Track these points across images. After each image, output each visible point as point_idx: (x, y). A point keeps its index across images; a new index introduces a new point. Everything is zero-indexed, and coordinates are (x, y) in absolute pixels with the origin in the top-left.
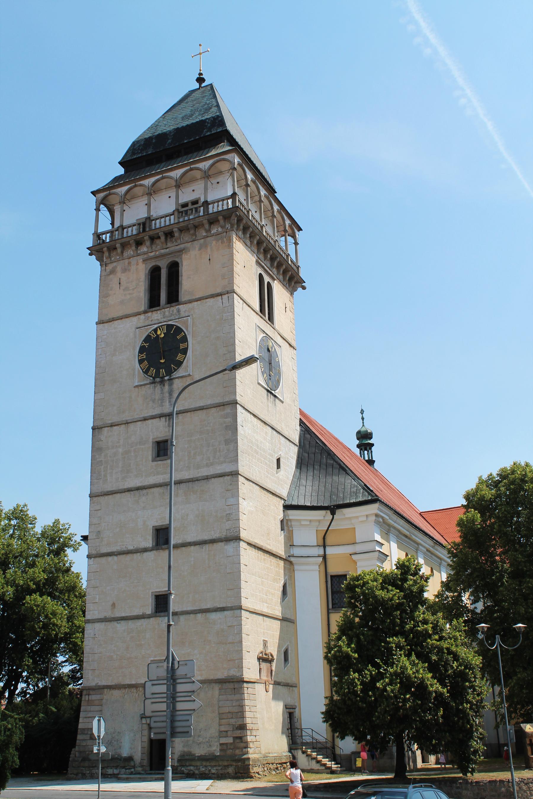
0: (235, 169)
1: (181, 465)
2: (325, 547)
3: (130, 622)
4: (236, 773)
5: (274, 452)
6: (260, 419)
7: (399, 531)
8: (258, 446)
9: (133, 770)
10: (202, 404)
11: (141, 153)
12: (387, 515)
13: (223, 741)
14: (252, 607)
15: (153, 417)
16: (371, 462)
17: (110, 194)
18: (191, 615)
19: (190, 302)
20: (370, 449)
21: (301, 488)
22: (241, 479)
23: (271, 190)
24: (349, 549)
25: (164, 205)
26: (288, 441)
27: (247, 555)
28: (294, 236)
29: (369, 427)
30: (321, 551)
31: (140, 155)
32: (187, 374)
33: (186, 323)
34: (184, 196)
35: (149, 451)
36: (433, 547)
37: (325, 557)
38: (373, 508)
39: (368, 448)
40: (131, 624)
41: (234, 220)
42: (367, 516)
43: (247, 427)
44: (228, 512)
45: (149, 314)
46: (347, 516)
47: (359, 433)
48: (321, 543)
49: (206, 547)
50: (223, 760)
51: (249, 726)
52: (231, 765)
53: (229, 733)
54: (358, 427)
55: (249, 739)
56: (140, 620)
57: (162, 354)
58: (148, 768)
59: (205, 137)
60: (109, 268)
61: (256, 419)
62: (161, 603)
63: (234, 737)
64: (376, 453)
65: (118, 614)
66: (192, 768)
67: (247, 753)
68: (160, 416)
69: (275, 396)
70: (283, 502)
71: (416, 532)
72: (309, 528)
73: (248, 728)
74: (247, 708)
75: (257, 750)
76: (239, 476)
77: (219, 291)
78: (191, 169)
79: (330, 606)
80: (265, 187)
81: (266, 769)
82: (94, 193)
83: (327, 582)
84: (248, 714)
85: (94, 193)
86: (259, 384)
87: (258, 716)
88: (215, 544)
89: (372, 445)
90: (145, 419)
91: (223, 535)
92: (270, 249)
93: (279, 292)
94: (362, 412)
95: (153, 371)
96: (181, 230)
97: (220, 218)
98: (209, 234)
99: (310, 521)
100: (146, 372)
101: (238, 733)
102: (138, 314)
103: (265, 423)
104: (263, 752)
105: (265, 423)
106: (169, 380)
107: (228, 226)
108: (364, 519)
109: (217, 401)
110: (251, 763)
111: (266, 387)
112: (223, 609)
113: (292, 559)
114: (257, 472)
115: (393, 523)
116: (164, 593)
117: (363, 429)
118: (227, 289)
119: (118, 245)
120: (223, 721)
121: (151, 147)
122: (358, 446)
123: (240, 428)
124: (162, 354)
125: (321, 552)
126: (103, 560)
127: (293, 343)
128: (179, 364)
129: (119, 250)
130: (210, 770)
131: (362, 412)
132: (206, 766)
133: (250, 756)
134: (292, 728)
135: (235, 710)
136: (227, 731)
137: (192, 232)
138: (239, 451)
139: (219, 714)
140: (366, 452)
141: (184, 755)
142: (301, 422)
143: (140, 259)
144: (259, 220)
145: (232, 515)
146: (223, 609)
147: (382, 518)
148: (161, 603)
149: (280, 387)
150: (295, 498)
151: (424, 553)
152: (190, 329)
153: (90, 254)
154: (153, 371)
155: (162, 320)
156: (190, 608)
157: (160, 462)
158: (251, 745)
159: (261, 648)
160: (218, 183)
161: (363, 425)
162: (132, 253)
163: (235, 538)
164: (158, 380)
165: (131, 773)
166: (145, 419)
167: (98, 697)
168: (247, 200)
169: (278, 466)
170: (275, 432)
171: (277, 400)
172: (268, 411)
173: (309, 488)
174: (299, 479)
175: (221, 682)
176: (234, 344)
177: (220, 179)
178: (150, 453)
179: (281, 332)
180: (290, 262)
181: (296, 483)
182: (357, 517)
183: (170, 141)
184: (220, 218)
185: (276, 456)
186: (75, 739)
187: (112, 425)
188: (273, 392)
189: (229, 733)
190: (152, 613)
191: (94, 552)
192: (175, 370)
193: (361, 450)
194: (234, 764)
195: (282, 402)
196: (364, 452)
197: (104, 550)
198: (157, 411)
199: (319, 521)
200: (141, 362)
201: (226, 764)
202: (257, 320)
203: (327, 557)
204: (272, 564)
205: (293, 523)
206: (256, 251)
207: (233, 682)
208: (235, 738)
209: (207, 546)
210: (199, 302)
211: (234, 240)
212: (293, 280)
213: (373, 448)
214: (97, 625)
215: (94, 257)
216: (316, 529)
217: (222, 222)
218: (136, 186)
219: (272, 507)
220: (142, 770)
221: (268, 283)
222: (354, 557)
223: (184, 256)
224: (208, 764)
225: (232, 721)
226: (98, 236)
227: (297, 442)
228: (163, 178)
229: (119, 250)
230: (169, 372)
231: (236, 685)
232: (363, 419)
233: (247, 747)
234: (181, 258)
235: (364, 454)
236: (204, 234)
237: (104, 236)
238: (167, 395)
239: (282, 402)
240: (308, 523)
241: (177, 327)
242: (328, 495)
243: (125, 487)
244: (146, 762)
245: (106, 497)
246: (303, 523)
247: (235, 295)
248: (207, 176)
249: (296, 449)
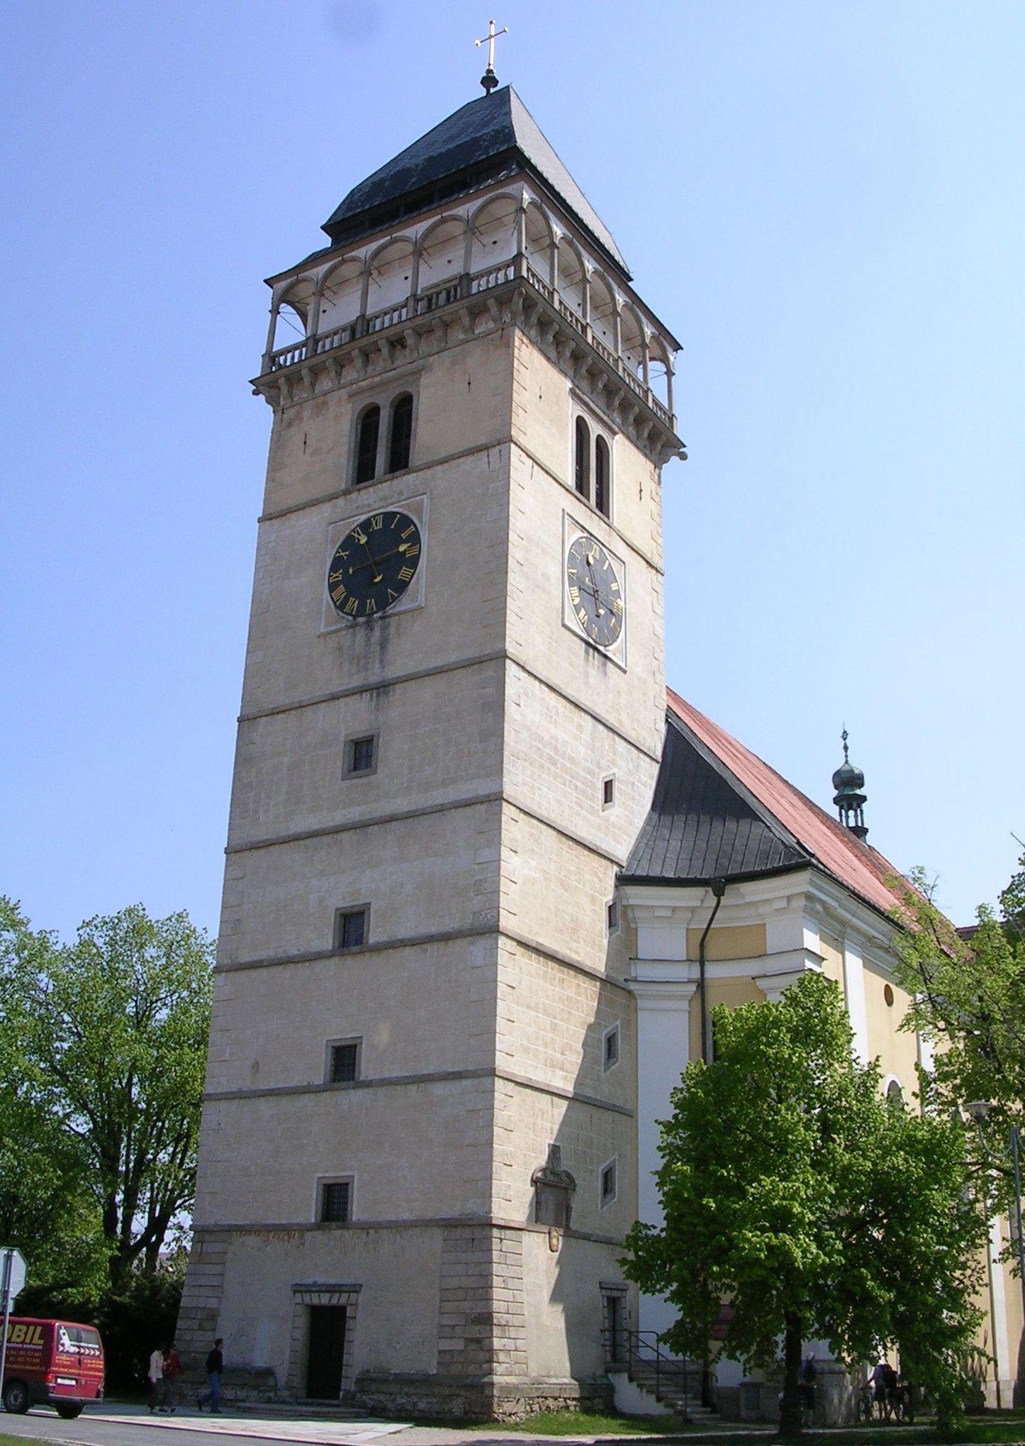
0: (522, 210)
1: (391, 788)
2: (702, 962)
3: (284, 1101)
4: (466, 1413)
5: (599, 767)
6: (565, 697)
8: (556, 750)
9: (272, 1394)
10: (440, 663)
13: (446, 1345)
14: (522, 1073)
15: (348, 694)
16: (860, 831)
17: (298, 282)
18: (398, 1087)
19: (429, 466)
20: (859, 806)
21: (659, 843)
22: (507, 810)
23: (623, 277)
24: (752, 968)
25: (392, 291)
26: (634, 750)
27: (512, 968)
29: (858, 765)
30: (695, 973)
32: (415, 605)
33: (419, 510)
34: (446, 282)
35: (337, 759)
37: (701, 985)
38: (800, 882)
39: (855, 805)
40: (285, 1103)
41: (518, 303)
42: (789, 898)
43: (525, 708)
44: (478, 877)
45: (354, 495)
46: (748, 899)
47: (837, 775)
48: (695, 953)
49: (432, 948)
50: (441, 1385)
51: (497, 1318)
52: (458, 1396)
53: (458, 1330)
54: (838, 764)
55: (497, 1343)
56: (302, 1097)
57: (373, 570)
58: (302, 1393)
60: (291, 413)
61: (553, 695)
62: (344, 1062)
63: (466, 1339)
64: (871, 814)
65: (263, 1085)
66: (381, 1397)
67: (491, 1372)
68: (361, 691)
69: (606, 657)
70: (616, 868)
72: (669, 922)
73: (495, 1321)
74: (496, 1281)
75: (517, 1369)
76: (504, 804)
77: (482, 440)
80: (595, 255)
81: (536, 1407)
84: (497, 1293)
86: (564, 626)
87: (524, 1297)
88: (450, 943)
89: (864, 799)
90: (334, 697)
91: (467, 922)
92: (602, 372)
93: (625, 457)
94: (845, 735)
95: (353, 603)
96: (419, 334)
97: (491, 302)
98: (471, 336)
99: (674, 909)
100: (341, 607)
101: (475, 1331)
102: (334, 497)
103: (577, 706)
104: (534, 1374)
105: (577, 706)
106: (381, 618)
107: (507, 318)
108: (783, 904)
109: (464, 657)
110: (495, 1392)
111: (584, 636)
112: (458, 1076)
113: (632, 986)
114: (553, 802)
115: (849, 916)
116: (348, 1043)
117: (847, 767)
118: (499, 436)
119: (305, 372)
122: (836, 801)
123: (510, 708)
124: (373, 570)
125: (696, 974)
126: (243, 976)
127: (656, 561)
128: (402, 586)
129: (307, 380)
130: (415, 1404)
131: (845, 735)
132: (408, 1395)
133: (496, 1379)
134: (618, 1327)
136: (454, 1326)
137: (439, 333)
138: (506, 753)
139: (442, 1290)
141: (368, 1371)
142: (670, 715)
143: (343, 393)
144: (547, 281)
145: (486, 884)
146: (458, 1076)
147: (823, 903)
148: (344, 1062)
149: (619, 640)
150: (645, 863)
152: (425, 518)
153: (255, 393)
154: (353, 603)
155: (376, 506)
156: (397, 1073)
158: (502, 1357)
161: (846, 762)
162: (330, 384)
163: (493, 930)
164: (361, 620)
165: (269, 1401)
166: (334, 697)
167: (218, 1247)
168: (582, 304)
169: (608, 797)
170: (601, 727)
171: (609, 664)
172: (587, 683)
173: (675, 844)
174: (657, 827)
175: (449, 1224)
176: (505, 541)
178: (339, 763)
179: (627, 534)
180: (650, 404)
181: (648, 838)
184: (491, 302)
185: (603, 775)
186: (174, 1327)
187: (274, 713)
188: (601, 648)
190: (325, 1084)
191: (226, 961)
192: (394, 599)
193: (841, 808)
194: (462, 1393)
195: (625, 672)
196: (847, 812)
197: (245, 957)
198: (356, 682)
199: (693, 910)
200: (332, 587)
201: (447, 1392)
203: (708, 983)
204: (582, 991)
205: (637, 914)
206: (571, 373)
207: (470, 1226)
208: (469, 1340)
209: (435, 945)
210: (446, 466)
211: (517, 343)
212: (659, 440)
213: (864, 806)
214: (223, 1105)
215: (262, 397)
216: (685, 926)
218: (344, 262)
219: (588, 877)
220: (291, 1396)
221: (599, 438)
223: (424, 380)
224: (412, 1391)
225: (465, 1305)
226: (271, 358)
227: (658, 754)
229: (307, 380)
230: (383, 604)
231: (478, 1233)
232: (846, 748)
233: (491, 1361)
235: (847, 817)
236: (462, 336)
237: (282, 359)
238: (378, 648)
239: (625, 672)
240: (669, 913)
241: (403, 515)
242: (711, 857)
243: (290, 832)
244: (298, 1381)
245: (256, 853)
247: (513, 446)
248: (472, 228)
249: (655, 769)
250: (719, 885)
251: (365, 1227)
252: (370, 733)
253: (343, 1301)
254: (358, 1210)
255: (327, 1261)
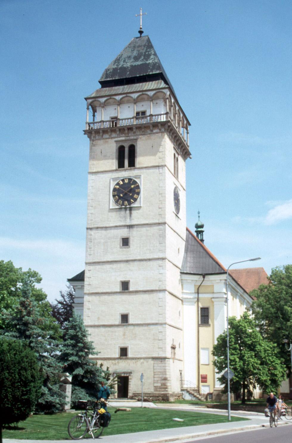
1: (135, 250)
2: (198, 293)
7: (232, 286)
11: (112, 77)
12: (230, 280)
13: (156, 385)
16: (202, 240)
20: (202, 233)
24: (210, 296)
28: (187, 129)
31: (111, 79)
35: (119, 242)
36: (243, 293)
38: (224, 277)
59: (149, 75)
62: (125, 318)
70: (180, 270)
71: (239, 288)
78: (143, 94)
79: (200, 323)
82: (86, 99)
83: (198, 311)
84: (168, 373)
85: (86, 99)
94: (199, 213)
98: (152, 132)
101: (163, 382)
120: (155, 376)
121: (118, 75)
128: (135, 200)
130: (149, 398)
131: (199, 213)
135: (162, 370)
139: (154, 372)
140: (200, 235)
148: (125, 318)
151: (239, 297)
153: (85, 134)
157: (124, 249)
159: (171, 343)
160: (157, 103)
177: (158, 101)
181: (185, 260)
182: (215, 280)
183: (128, 73)
184: (159, 125)
189: (159, 382)
192: (133, 203)
199: (196, 281)
202: (174, 179)
213: (204, 233)
217: (160, 127)
222: (213, 299)
225: (161, 376)
228: (127, 96)
229: (101, 134)
234: (137, 143)
246: (188, 281)
250: (204, 276)
251: (133, 359)
252: (128, 237)
253: (127, 375)
254: (130, 354)
255: (122, 367)
